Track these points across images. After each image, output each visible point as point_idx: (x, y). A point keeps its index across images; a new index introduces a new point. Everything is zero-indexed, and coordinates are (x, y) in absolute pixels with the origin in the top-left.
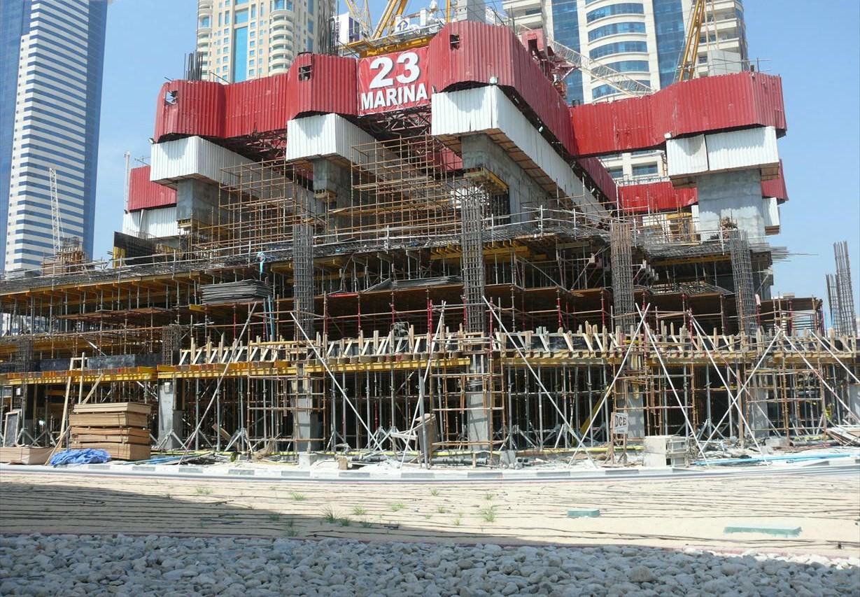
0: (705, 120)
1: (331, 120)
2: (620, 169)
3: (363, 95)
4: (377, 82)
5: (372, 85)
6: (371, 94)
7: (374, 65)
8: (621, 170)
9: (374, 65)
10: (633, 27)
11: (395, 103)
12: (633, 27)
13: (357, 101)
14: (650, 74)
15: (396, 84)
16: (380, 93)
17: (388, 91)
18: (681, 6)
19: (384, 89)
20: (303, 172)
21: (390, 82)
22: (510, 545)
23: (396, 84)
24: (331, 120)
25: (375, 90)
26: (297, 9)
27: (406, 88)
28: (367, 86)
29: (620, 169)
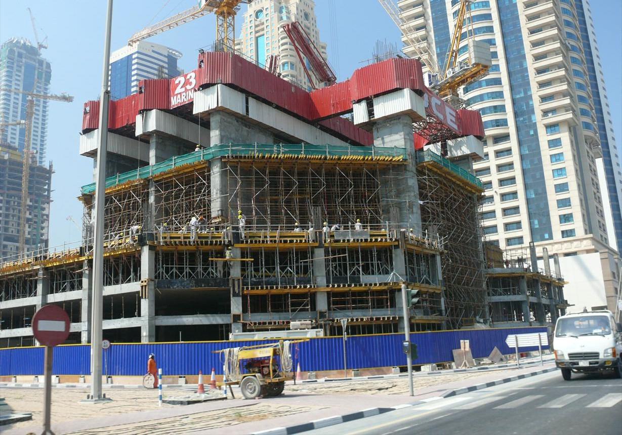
0: (370, 90)
1: (407, 91)
2: (490, 183)
3: (172, 98)
4: (178, 90)
5: (177, 92)
6: (175, 97)
7: (177, 82)
8: (489, 169)
9: (177, 82)
10: (496, 109)
11: (185, 100)
12: (496, 109)
13: (169, 102)
14: (503, 87)
15: (186, 90)
16: (179, 96)
17: (183, 94)
18: (527, 72)
19: (180, 94)
20: (146, 138)
21: (183, 89)
22: (257, 358)
23: (186, 90)
24: (407, 91)
25: (177, 95)
26: (298, 69)
27: (190, 92)
28: (173, 93)
29: (490, 183)
